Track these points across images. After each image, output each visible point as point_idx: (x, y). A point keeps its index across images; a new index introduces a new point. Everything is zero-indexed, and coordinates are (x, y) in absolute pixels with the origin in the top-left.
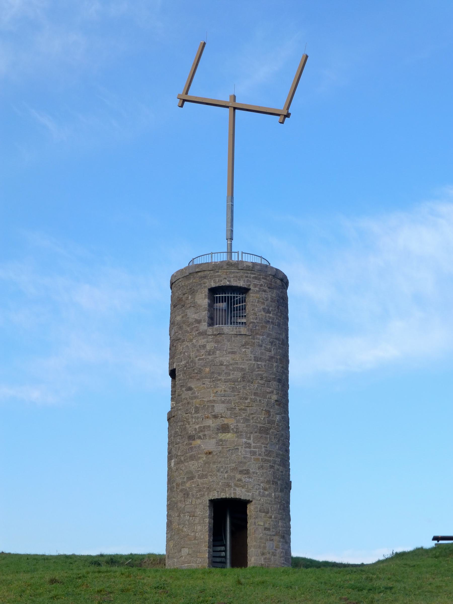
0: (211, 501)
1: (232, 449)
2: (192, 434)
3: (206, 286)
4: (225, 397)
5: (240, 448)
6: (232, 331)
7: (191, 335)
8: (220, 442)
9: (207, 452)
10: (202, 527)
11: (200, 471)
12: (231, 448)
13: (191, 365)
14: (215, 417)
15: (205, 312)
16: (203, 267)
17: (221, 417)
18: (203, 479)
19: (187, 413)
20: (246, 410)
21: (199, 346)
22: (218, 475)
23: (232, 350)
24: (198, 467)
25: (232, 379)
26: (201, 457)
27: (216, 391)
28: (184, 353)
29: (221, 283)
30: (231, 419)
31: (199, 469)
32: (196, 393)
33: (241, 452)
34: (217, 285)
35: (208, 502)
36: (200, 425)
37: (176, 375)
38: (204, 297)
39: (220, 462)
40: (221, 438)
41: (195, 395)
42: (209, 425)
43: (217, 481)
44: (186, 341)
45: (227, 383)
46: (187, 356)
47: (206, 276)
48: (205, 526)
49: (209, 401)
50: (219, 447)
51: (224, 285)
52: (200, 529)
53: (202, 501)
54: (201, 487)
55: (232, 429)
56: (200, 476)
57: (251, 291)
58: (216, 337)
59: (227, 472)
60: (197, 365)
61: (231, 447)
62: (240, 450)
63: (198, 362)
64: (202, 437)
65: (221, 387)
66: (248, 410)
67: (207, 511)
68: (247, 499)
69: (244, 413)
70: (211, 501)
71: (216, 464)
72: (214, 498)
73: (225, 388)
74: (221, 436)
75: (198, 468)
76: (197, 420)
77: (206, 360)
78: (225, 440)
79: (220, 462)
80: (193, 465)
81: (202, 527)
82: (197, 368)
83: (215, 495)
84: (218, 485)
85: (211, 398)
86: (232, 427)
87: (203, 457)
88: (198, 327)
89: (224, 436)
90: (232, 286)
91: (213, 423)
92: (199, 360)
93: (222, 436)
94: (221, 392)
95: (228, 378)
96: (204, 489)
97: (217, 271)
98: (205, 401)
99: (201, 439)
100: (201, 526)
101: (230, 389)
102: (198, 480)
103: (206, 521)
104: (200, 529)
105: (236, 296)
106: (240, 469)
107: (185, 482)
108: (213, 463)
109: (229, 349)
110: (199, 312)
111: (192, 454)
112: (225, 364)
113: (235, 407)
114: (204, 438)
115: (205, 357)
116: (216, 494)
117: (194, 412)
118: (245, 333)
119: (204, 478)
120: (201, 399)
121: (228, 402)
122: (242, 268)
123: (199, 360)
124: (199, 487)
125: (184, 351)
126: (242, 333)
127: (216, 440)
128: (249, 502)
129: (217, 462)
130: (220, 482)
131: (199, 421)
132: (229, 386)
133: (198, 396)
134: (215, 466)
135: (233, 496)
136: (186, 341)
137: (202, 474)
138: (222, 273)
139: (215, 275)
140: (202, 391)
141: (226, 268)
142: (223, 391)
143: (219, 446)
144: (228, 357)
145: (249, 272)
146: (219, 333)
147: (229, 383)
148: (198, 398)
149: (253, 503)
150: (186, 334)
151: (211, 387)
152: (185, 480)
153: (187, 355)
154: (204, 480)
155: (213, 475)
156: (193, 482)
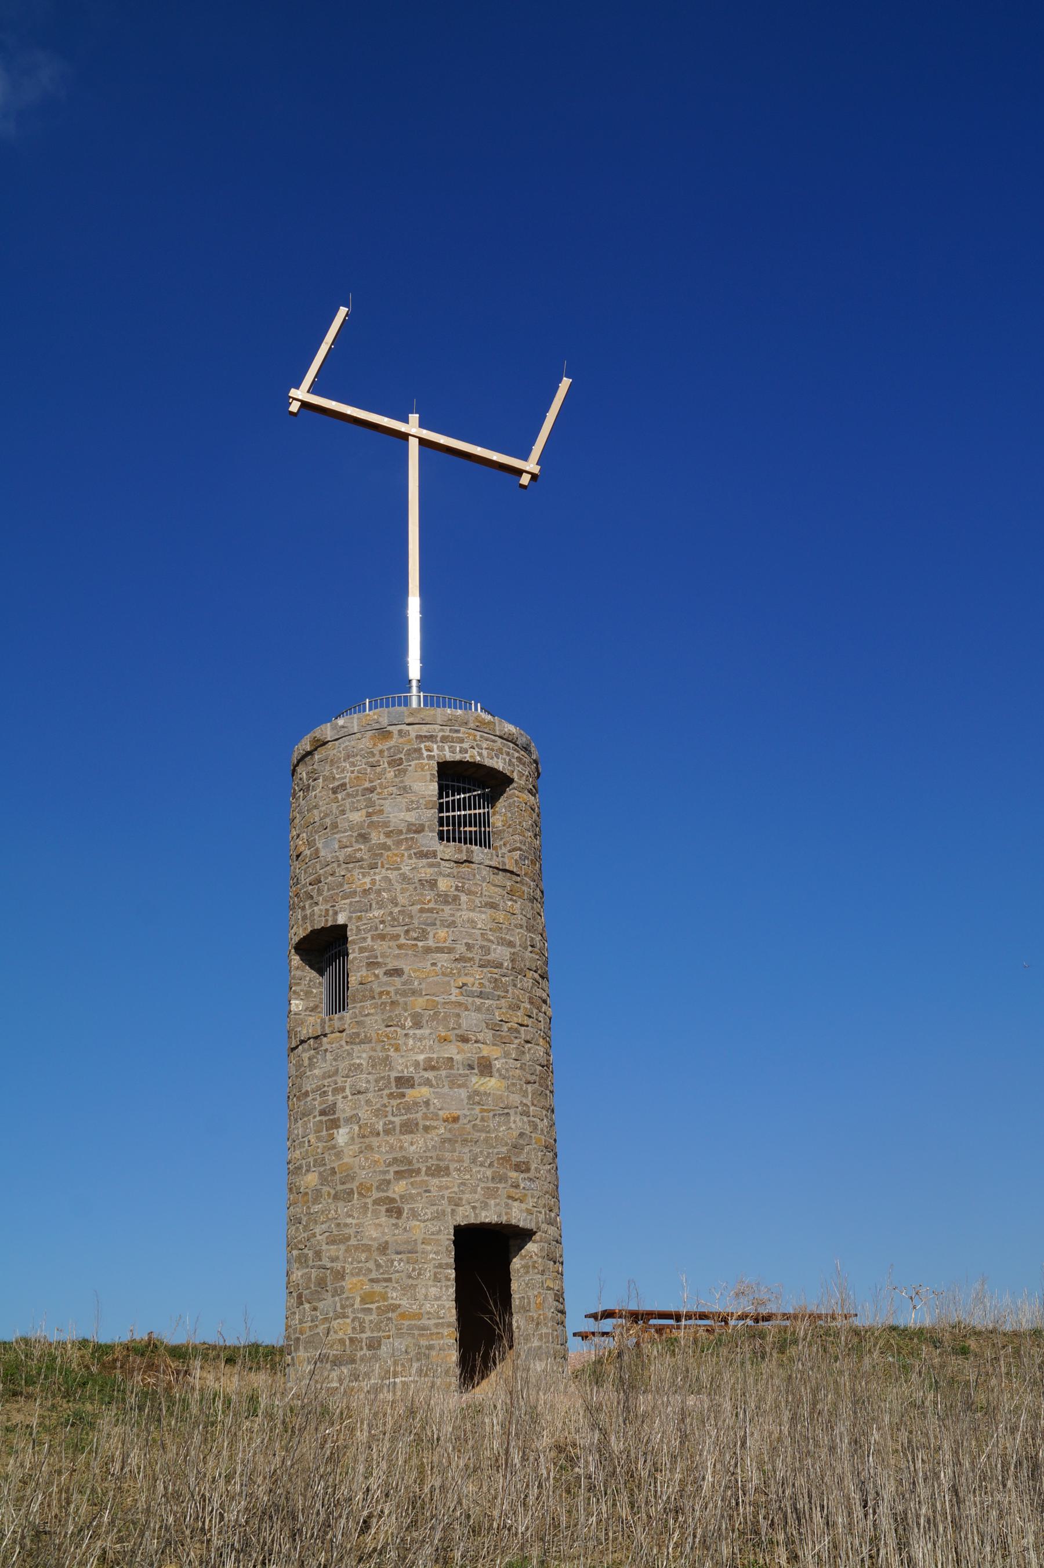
0: (459, 1230)
1: (499, 1114)
2: (406, 1072)
3: (434, 756)
4: (481, 998)
5: (512, 1112)
6: (491, 860)
7: (396, 855)
8: (476, 1097)
9: (449, 1116)
10: (441, 1289)
11: (431, 1157)
12: (498, 1112)
13: (401, 920)
14: (465, 1040)
15: (433, 811)
16: (425, 716)
17: (476, 1042)
18: (439, 1177)
19: (389, 1024)
20: (519, 1032)
21: (420, 880)
22: (474, 1170)
23: (491, 901)
24: (425, 1149)
25: (494, 961)
26: (432, 1126)
27: (463, 984)
28: (378, 892)
29: (466, 755)
30: (495, 1047)
31: (428, 1154)
32: (416, 983)
33: (515, 1122)
34: (458, 757)
35: (452, 1231)
36: (428, 1055)
37: (347, 938)
38: (428, 777)
39: (477, 1141)
40: (476, 1086)
41: (410, 987)
42: (450, 1056)
43: (471, 1184)
44: (383, 867)
45: (485, 970)
46: (388, 899)
47: (432, 736)
48: (447, 1287)
49: (448, 1003)
50: (474, 1107)
51: (472, 760)
52: (434, 1295)
53: (439, 1227)
54: (434, 1196)
55: (498, 1070)
56: (431, 1169)
57: (515, 785)
58: (460, 866)
59: (491, 1165)
60: (416, 921)
61: (496, 1108)
62: (512, 1118)
63: (419, 915)
64: (434, 1082)
65: (472, 975)
66: (522, 1032)
67: (450, 1251)
68: (528, 1226)
69: (516, 1038)
70: (459, 1230)
71: (469, 1144)
72: (465, 1223)
73: (482, 979)
74: (477, 1082)
75: (425, 1151)
76: (419, 1043)
77: (437, 912)
78: (485, 1093)
79: (477, 1141)
80: (412, 1144)
81: (441, 1289)
82: (417, 928)
83: (466, 1216)
84: (476, 1193)
85: (453, 998)
86: (498, 1066)
87: (436, 1128)
88: (416, 840)
89: (482, 1084)
90: (485, 765)
91: (458, 1053)
92: (422, 911)
93: (476, 1081)
94: (473, 985)
95: (484, 957)
96: (444, 1200)
97: (456, 728)
98: (438, 1003)
99: (431, 1086)
100: (437, 1287)
101: (490, 983)
102: (426, 1178)
103: (451, 1275)
104: (434, 1295)
105: (468, 788)
106: (515, 1159)
107: (389, 1182)
108: (462, 1141)
109: (485, 896)
110: (417, 808)
111: (409, 1119)
112: (479, 926)
113: (500, 1023)
114: (437, 1084)
115: (434, 907)
116: (469, 1211)
117: (411, 1024)
118: (511, 869)
119: (443, 1176)
120: (428, 997)
121: (489, 1010)
122: (502, 734)
123: (422, 911)
124: (430, 1196)
125: (377, 887)
126: (507, 868)
127: (468, 1092)
128: (525, 1235)
129: (471, 1141)
130: (478, 1186)
131: (425, 1046)
132: (489, 975)
133: (421, 990)
134: (466, 1150)
135: (504, 1220)
136: (383, 867)
137: (437, 1165)
138: (467, 735)
139: (453, 738)
140: (431, 979)
141: (475, 727)
142: (477, 985)
143: (474, 1104)
144: (485, 913)
145: (512, 745)
146: (465, 858)
147: (488, 969)
148: (421, 995)
149: (537, 1237)
150: (383, 851)
151: (451, 973)
152: (390, 1176)
153: (386, 897)
154: (441, 1179)
155: (462, 1168)
156: (412, 1184)
